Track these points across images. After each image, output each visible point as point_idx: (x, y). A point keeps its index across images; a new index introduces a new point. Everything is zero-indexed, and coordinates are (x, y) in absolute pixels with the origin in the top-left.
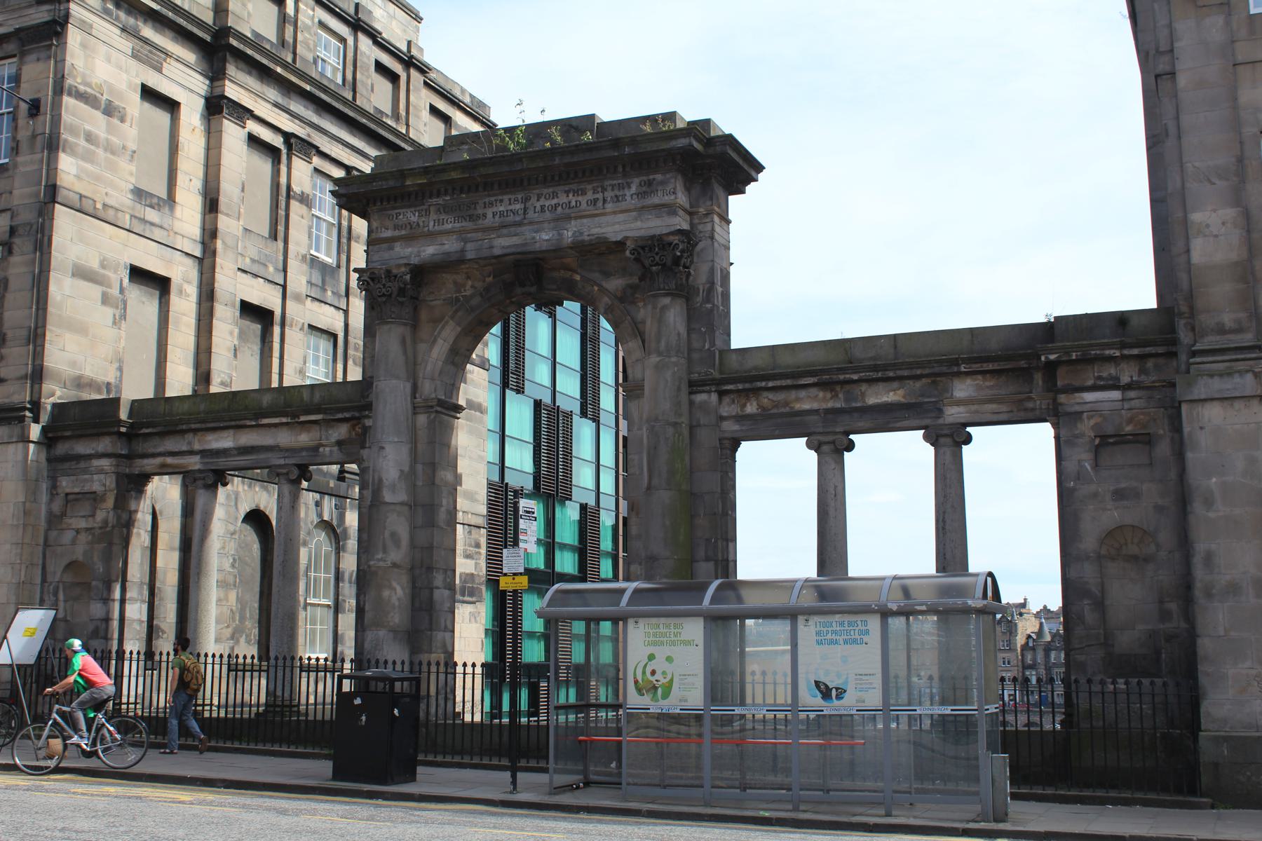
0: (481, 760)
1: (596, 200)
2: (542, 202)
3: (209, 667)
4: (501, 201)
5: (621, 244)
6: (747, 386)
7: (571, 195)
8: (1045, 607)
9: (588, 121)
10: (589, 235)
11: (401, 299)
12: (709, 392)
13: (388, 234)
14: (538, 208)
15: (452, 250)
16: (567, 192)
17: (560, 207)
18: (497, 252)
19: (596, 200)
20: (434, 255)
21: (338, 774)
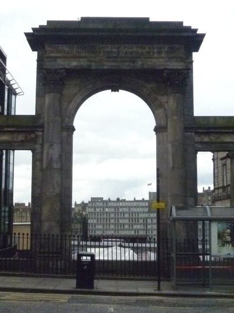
0: (130, 277)
1: (149, 52)
2: (126, 49)
3: (21, 240)
4: (108, 47)
5: (162, 71)
6: (207, 131)
7: (139, 49)
8: (83, 202)
9: (146, 20)
10: (147, 66)
11: (60, 82)
12: (191, 132)
13: (54, 55)
14: (124, 52)
15: (84, 64)
16: (137, 47)
17: (134, 54)
18: (105, 67)
19: (149, 52)
20: (76, 66)
21: (79, 285)
